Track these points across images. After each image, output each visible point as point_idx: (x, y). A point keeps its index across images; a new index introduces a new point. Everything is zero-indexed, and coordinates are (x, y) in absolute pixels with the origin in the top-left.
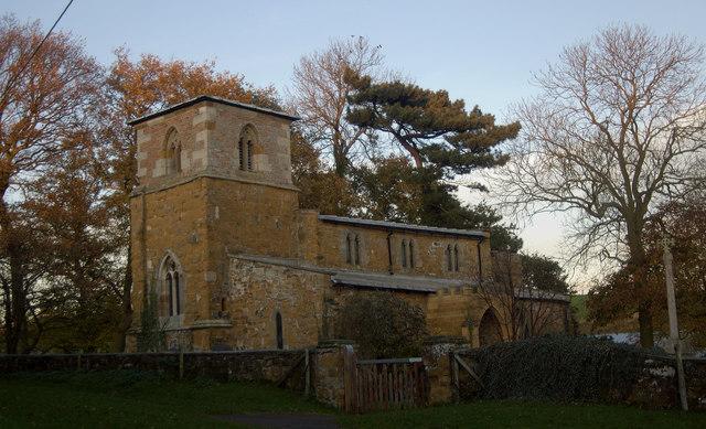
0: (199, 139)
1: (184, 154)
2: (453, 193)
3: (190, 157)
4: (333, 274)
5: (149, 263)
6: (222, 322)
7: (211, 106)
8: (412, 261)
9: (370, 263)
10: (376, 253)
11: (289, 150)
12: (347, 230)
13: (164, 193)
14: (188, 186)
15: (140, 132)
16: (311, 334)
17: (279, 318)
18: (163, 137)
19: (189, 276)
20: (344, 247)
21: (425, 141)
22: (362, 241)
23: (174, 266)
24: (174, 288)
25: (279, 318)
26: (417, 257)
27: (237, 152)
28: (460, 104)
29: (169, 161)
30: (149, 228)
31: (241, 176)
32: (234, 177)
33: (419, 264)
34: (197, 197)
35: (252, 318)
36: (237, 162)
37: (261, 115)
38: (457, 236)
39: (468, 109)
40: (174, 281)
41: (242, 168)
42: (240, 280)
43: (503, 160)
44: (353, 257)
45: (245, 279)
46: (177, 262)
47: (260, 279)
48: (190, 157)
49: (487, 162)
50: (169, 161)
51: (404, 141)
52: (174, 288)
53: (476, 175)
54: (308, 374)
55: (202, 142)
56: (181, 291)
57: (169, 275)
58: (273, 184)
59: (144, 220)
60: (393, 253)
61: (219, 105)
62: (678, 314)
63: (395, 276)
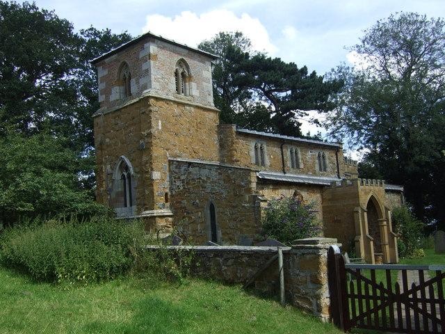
1: (133, 81)
3: (138, 83)
7: (154, 42)
9: (271, 166)
10: (274, 158)
13: (118, 113)
14: (137, 106)
15: (100, 69)
17: (212, 208)
18: (117, 70)
19: (139, 176)
20: (253, 153)
23: (127, 168)
24: (127, 186)
25: (212, 208)
26: (300, 161)
27: (173, 79)
29: (122, 88)
32: (171, 98)
33: (302, 166)
36: (174, 87)
37: (190, 53)
39: (309, 73)
42: (179, 178)
45: (182, 178)
46: (129, 164)
47: (195, 177)
48: (138, 83)
50: (122, 88)
51: (268, 94)
52: (127, 186)
56: (132, 187)
57: (123, 175)
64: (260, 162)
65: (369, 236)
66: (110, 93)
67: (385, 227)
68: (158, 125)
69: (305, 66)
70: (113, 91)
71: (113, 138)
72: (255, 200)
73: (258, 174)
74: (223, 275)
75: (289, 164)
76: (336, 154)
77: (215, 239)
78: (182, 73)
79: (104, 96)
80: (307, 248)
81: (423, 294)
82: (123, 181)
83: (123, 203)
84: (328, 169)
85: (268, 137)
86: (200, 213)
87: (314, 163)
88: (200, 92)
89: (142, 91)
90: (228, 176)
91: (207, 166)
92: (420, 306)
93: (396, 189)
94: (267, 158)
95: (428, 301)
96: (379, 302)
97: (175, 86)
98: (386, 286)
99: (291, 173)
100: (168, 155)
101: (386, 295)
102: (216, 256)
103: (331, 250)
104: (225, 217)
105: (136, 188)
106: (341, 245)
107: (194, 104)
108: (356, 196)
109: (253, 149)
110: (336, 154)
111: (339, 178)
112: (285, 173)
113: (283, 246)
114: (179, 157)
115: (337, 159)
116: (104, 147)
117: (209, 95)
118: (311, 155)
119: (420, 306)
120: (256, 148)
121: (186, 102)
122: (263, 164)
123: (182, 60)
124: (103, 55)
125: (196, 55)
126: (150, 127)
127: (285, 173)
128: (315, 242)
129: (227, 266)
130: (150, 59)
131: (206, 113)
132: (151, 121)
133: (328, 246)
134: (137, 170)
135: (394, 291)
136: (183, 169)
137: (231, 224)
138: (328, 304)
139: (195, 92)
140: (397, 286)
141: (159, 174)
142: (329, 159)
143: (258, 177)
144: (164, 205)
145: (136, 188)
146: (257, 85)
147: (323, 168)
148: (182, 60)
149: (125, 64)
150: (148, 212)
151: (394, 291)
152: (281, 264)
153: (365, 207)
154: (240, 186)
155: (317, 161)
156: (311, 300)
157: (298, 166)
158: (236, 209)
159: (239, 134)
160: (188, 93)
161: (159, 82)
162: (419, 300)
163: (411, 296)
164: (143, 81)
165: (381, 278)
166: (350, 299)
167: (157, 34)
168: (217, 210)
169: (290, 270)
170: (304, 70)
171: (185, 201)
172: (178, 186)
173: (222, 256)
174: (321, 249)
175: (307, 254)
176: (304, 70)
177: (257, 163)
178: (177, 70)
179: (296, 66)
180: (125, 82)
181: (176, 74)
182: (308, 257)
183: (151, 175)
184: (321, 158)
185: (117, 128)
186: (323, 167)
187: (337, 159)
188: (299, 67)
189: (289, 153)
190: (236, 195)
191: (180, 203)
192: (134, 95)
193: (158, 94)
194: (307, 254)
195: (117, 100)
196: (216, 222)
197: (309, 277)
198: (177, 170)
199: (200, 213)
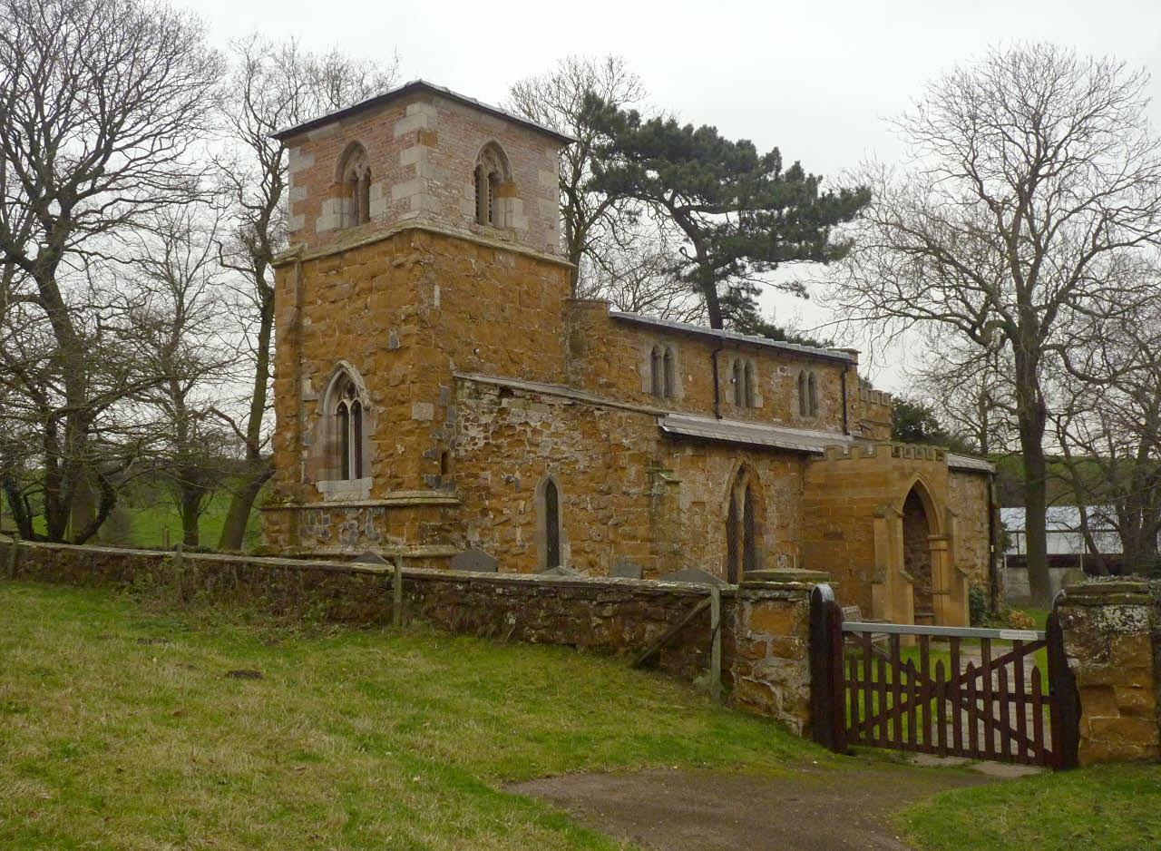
0: (404, 162)
1: (376, 190)
3: (387, 193)
4: (662, 416)
5: (307, 386)
6: (440, 496)
7: (430, 102)
8: (747, 395)
9: (686, 400)
10: (696, 382)
12: (652, 341)
13: (336, 262)
14: (382, 247)
17: (550, 490)
19: (381, 409)
20: (646, 369)
21: (709, 217)
22: (676, 362)
23: (352, 390)
25: (550, 490)
26: (756, 390)
29: (346, 201)
30: (307, 322)
31: (476, 233)
32: (466, 234)
33: (759, 402)
34: (399, 266)
39: (786, 166)
40: (351, 419)
42: (476, 420)
43: (839, 253)
45: (485, 419)
50: (346, 201)
51: (680, 216)
53: (791, 271)
55: (411, 168)
56: (365, 433)
57: (343, 406)
58: (531, 252)
59: (299, 308)
61: (442, 102)
62: (971, 610)
63: (724, 422)
64: (662, 391)
65: (904, 572)
66: (318, 211)
67: (944, 555)
68: (432, 297)
71: (322, 318)
75: (729, 396)
76: (842, 377)
78: (491, 176)
79: (302, 218)
81: (987, 682)
82: (341, 418)
83: (340, 471)
84: (821, 412)
87: (788, 396)
88: (531, 222)
89: (397, 214)
91: (544, 398)
92: (980, 704)
95: (995, 696)
96: (904, 698)
98: (918, 669)
99: (733, 418)
100: (452, 366)
101: (918, 684)
105: (372, 438)
107: (514, 248)
109: (649, 361)
110: (842, 377)
111: (846, 433)
112: (719, 417)
114: (477, 371)
118: (781, 377)
119: (980, 704)
120: (654, 357)
121: (499, 244)
122: (669, 394)
123: (493, 145)
131: (544, 271)
135: (933, 677)
136: (486, 400)
137: (595, 530)
138: (807, 697)
139: (519, 222)
140: (940, 667)
142: (825, 388)
144: (438, 480)
146: (651, 193)
147: (809, 409)
148: (493, 145)
150: (401, 494)
151: (933, 677)
155: (795, 392)
156: (773, 689)
160: (502, 223)
161: (438, 195)
162: (978, 695)
163: (964, 687)
165: (910, 654)
166: (848, 690)
167: (438, 81)
168: (561, 498)
170: (773, 159)
171: (488, 474)
172: (473, 438)
176: (773, 159)
177: (655, 393)
178: (478, 168)
179: (752, 148)
184: (806, 384)
185: (332, 295)
186: (808, 406)
188: (762, 151)
189: (730, 372)
191: (476, 476)
192: (377, 222)
196: (560, 523)
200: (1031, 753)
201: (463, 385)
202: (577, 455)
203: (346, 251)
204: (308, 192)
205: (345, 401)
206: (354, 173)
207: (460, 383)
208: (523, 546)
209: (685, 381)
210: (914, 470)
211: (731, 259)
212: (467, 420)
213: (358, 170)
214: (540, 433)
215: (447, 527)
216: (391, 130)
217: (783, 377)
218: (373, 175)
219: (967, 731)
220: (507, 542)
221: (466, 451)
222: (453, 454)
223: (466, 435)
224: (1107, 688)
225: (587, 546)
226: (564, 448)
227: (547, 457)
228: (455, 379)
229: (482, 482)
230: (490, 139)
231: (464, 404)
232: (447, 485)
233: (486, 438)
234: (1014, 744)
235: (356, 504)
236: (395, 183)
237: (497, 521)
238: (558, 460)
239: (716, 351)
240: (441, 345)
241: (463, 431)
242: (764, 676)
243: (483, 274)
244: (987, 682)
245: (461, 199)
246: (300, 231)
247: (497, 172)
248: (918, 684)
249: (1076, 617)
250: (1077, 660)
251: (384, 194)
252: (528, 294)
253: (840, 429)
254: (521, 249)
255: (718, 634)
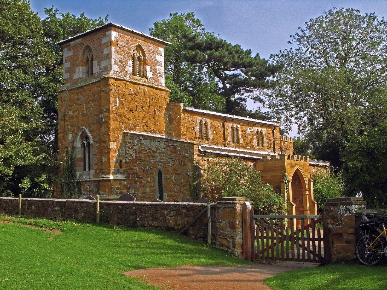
1: (95, 63)
2: (243, 103)
3: (99, 64)
9: (213, 140)
10: (217, 133)
11: (163, 64)
13: (81, 90)
14: (97, 84)
16: (184, 186)
17: (160, 174)
19: (97, 144)
23: (87, 138)
25: (160, 174)
26: (240, 137)
27: (130, 63)
28: (249, 52)
29: (85, 68)
32: (128, 78)
33: (241, 141)
35: (140, 173)
38: (262, 125)
39: (253, 55)
41: (134, 74)
42: (132, 148)
44: (204, 135)
45: (135, 148)
46: (89, 134)
48: (99, 64)
49: (263, 86)
50: (85, 68)
54: (210, 225)
56: (91, 156)
57: (83, 144)
58: (154, 86)
60: (226, 133)
68: (116, 102)
69: (250, 50)
70: (77, 70)
72: (196, 168)
73: (200, 147)
74: (166, 222)
75: (230, 139)
76: (273, 132)
77: (161, 198)
78: (139, 58)
79: (68, 74)
80: (227, 203)
81: (303, 234)
82: (83, 148)
84: (266, 145)
85: (212, 115)
86: (149, 179)
87: (252, 139)
90: (175, 148)
93: (322, 164)
94: (210, 133)
97: (132, 68)
101: (280, 236)
102: (162, 209)
103: (244, 206)
104: (171, 183)
105: (94, 155)
106: (252, 202)
108: (284, 168)
112: (225, 147)
113: (211, 202)
114: (133, 129)
115: (274, 136)
116: (67, 118)
117: (161, 76)
119: (301, 242)
121: (141, 83)
124: (69, 38)
125: (152, 41)
126: (109, 104)
127: (225, 147)
128: (234, 199)
129: (170, 216)
130: (111, 45)
132: (110, 99)
133: (242, 202)
134: (96, 139)
141: (116, 144)
143: (199, 150)
144: (118, 170)
145: (94, 155)
147: (261, 144)
149: (88, 47)
152: (209, 215)
153: (290, 178)
154: (184, 157)
155: (255, 137)
156: (229, 240)
157: (238, 142)
158: (180, 176)
159: (185, 111)
161: (118, 65)
162: (300, 239)
163: (295, 236)
164: (104, 64)
168: (164, 176)
169: (216, 219)
172: (131, 155)
173: (166, 209)
174: (237, 204)
175: (228, 208)
177: (201, 138)
178: (134, 54)
180: (89, 63)
181: (133, 58)
182: (228, 209)
183: (108, 145)
187: (274, 136)
190: (180, 164)
192: (96, 75)
193: (118, 76)
194: (228, 208)
195: (80, 78)
197: (228, 224)
198: (131, 141)
199: (149, 179)
200: (317, 259)
201: (127, 135)
202: (170, 161)
203: (84, 86)
204: (70, 64)
205: (84, 142)
206: (88, 57)
207: (126, 134)
208: (150, 195)
209: (213, 133)
210: (296, 164)
211: (236, 88)
212: (129, 148)
213: (89, 56)
214: (156, 152)
215: (122, 188)
216: (101, 41)
217: (250, 131)
218: (94, 58)
219: (147, 202)
220: (144, 193)
221: (129, 159)
222: (124, 161)
223: (129, 154)
224: (341, 235)
225: (173, 194)
226: (164, 158)
227: (158, 161)
228: (124, 133)
229: (135, 171)
230: (138, 44)
231: (128, 142)
232: (121, 172)
233: (136, 155)
234: (312, 256)
235: (88, 180)
236: (102, 61)
237: (140, 185)
238: (162, 162)
239: (224, 122)
240: (119, 120)
241: (128, 152)
242: (226, 235)
243: (135, 94)
244: (303, 234)
245: (127, 66)
246: (68, 79)
247: (141, 56)
248: (280, 236)
249: (330, 209)
250: (331, 225)
251: (98, 65)
252: (152, 101)
253: (272, 151)
254: (149, 85)
255: (210, 221)
